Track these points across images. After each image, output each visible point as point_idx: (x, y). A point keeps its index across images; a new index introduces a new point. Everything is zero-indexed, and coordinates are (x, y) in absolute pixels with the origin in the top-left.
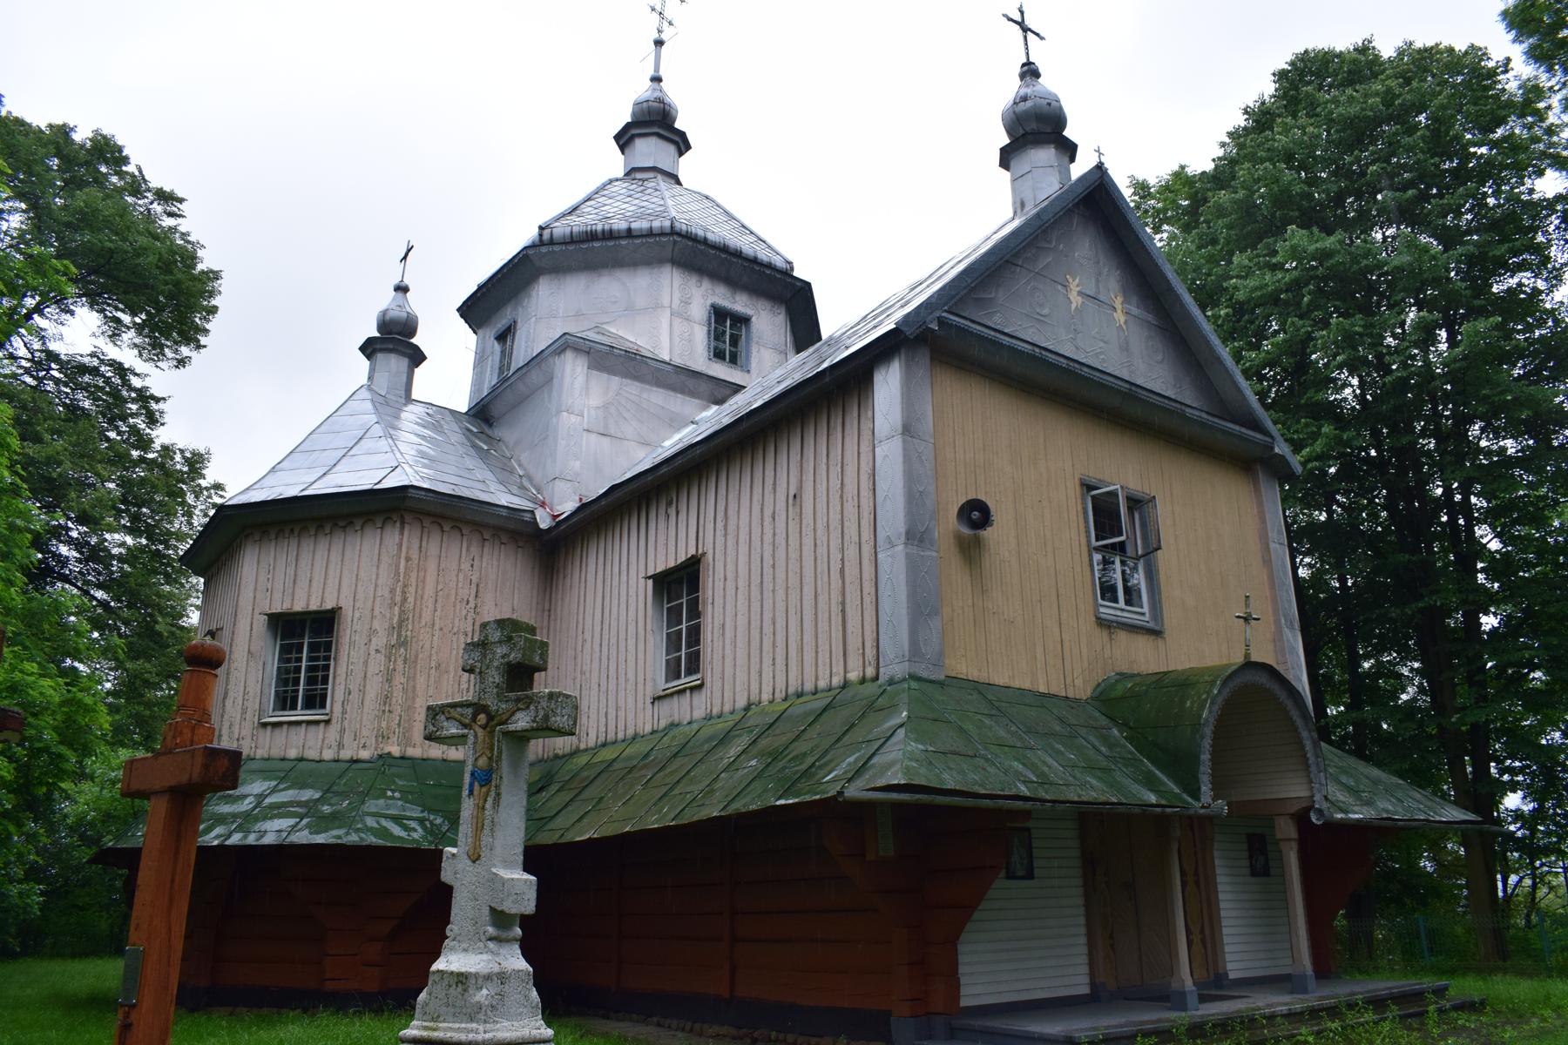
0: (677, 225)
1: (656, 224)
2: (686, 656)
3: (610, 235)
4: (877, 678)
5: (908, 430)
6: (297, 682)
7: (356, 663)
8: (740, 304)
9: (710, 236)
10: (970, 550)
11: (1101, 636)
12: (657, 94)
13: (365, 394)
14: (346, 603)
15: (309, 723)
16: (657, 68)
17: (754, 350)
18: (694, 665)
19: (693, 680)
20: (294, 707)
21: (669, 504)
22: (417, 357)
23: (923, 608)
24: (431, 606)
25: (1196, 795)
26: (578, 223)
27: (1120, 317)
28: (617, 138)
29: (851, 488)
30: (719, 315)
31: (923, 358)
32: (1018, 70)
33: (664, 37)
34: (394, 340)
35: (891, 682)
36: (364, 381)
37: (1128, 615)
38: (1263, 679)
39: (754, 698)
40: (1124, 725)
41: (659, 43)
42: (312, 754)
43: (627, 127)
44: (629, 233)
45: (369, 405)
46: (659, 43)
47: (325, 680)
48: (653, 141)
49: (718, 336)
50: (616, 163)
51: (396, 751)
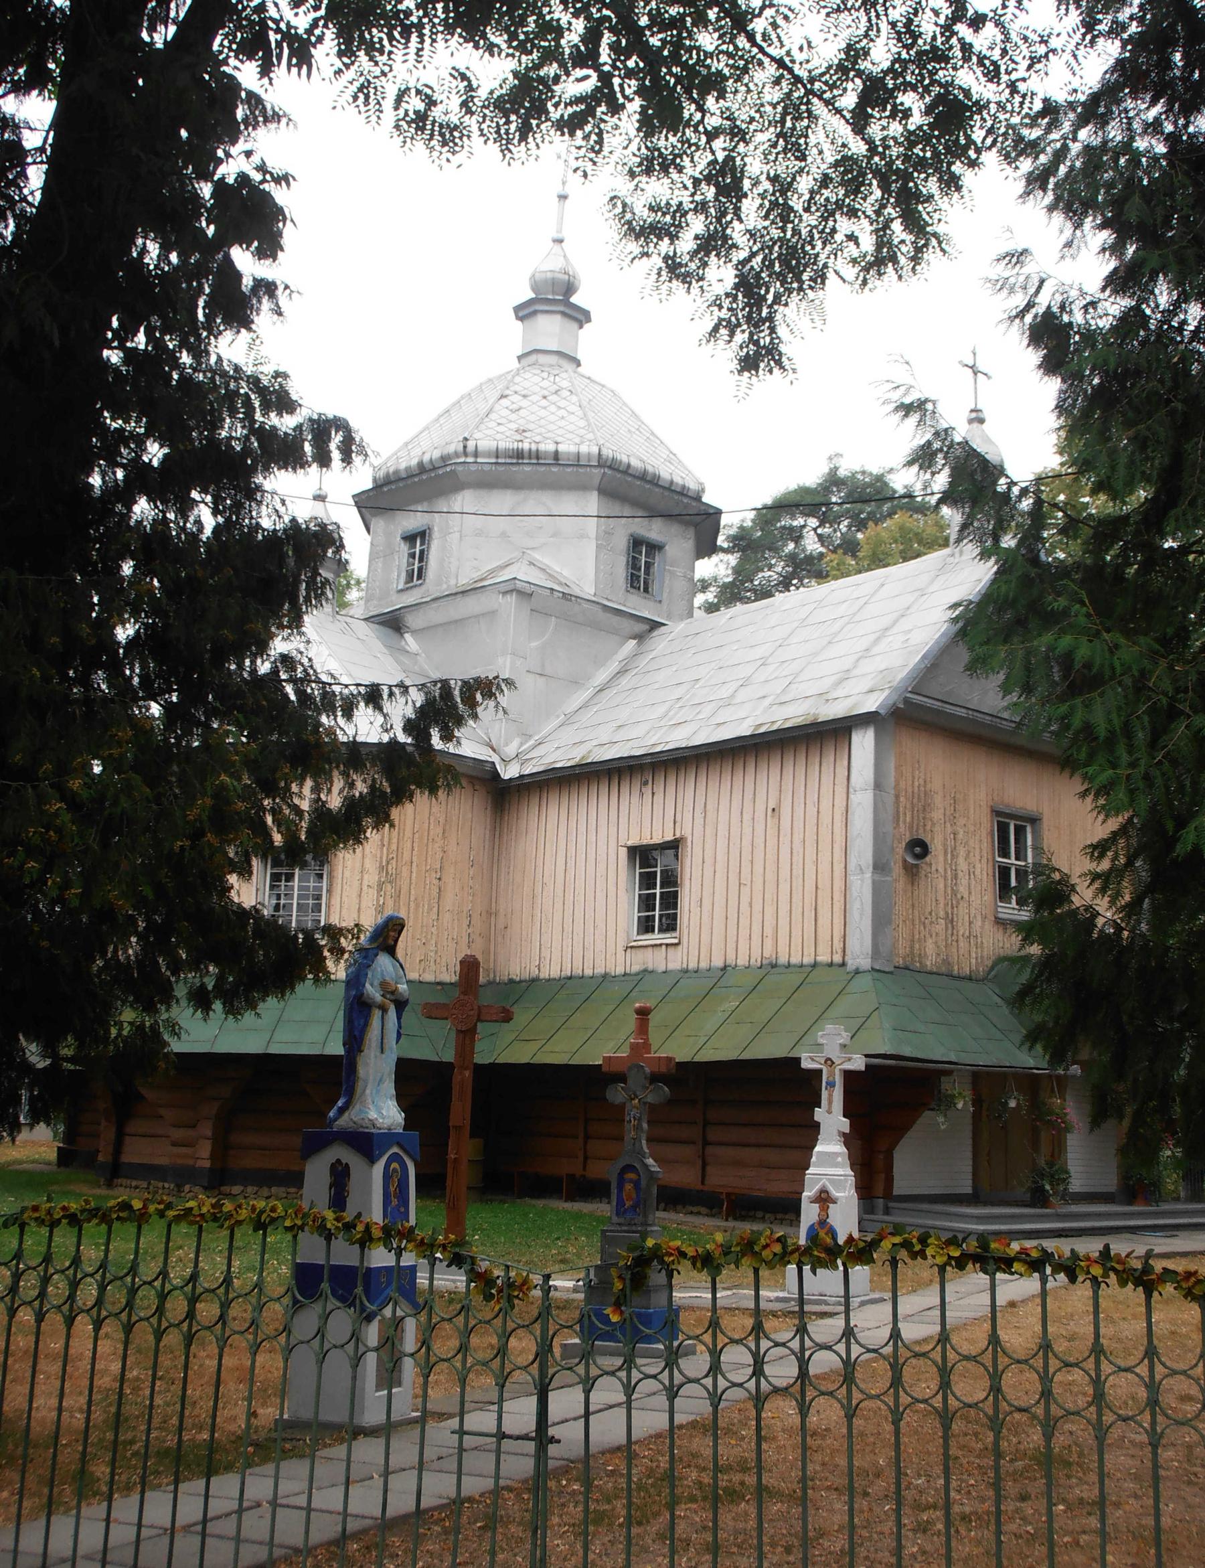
0: (605, 452)
1: (584, 449)
4: (843, 964)
5: (878, 786)
8: (654, 531)
9: (635, 463)
10: (912, 872)
16: (559, 231)
19: (668, 938)
23: (881, 919)
24: (409, 844)
26: (495, 436)
29: (826, 819)
33: (567, 190)
35: (857, 972)
39: (731, 960)
41: (563, 197)
43: (531, 302)
48: (558, 317)
49: (634, 564)
50: (514, 335)
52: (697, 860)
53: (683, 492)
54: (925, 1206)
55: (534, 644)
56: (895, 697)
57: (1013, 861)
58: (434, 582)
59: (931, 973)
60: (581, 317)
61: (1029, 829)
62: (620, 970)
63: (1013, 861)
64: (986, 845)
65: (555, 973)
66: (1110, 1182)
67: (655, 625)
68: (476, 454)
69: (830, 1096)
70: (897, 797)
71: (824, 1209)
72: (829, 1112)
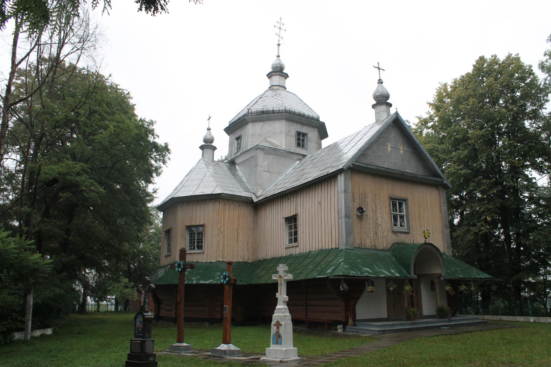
0: (287, 109)
1: (281, 109)
2: (294, 237)
3: (268, 112)
5: (345, 191)
6: (194, 243)
7: (209, 240)
8: (304, 130)
9: (296, 111)
10: (360, 218)
11: (394, 236)
12: (279, 62)
13: (202, 161)
14: (206, 223)
15: (199, 253)
16: (278, 53)
17: (309, 142)
18: (296, 240)
19: (296, 244)
20: (194, 249)
21: (288, 199)
22: (214, 148)
23: (349, 233)
25: (410, 274)
26: (258, 107)
27: (402, 152)
28: (267, 75)
30: (299, 134)
31: (349, 173)
32: (377, 81)
33: (280, 43)
34: (208, 145)
35: (342, 250)
36: (201, 157)
37: (402, 229)
38: (429, 246)
39: (311, 250)
40: (395, 257)
41: (279, 45)
42: (200, 261)
43: (270, 73)
44: (273, 112)
45: (204, 165)
46: (279, 45)
47: (202, 242)
48: (278, 76)
49: (299, 139)
51: (221, 260)
52: (302, 220)
53: (313, 118)
54: (366, 323)
55: (265, 163)
56: (349, 163)
57: (398, 213)
58: (243, 149)
59: (368, 249)
60: (286, 76)
61: (404, 203)
62: (284, 255)
63: (398, 213)
64: (388, 208)
65: (270, 258)
66: (433, 313)
67: (304, 156)
68: (251, 113)
69: (281, 289)
70: (353, 196)
71: (278, 328)
72: (281, 294)
